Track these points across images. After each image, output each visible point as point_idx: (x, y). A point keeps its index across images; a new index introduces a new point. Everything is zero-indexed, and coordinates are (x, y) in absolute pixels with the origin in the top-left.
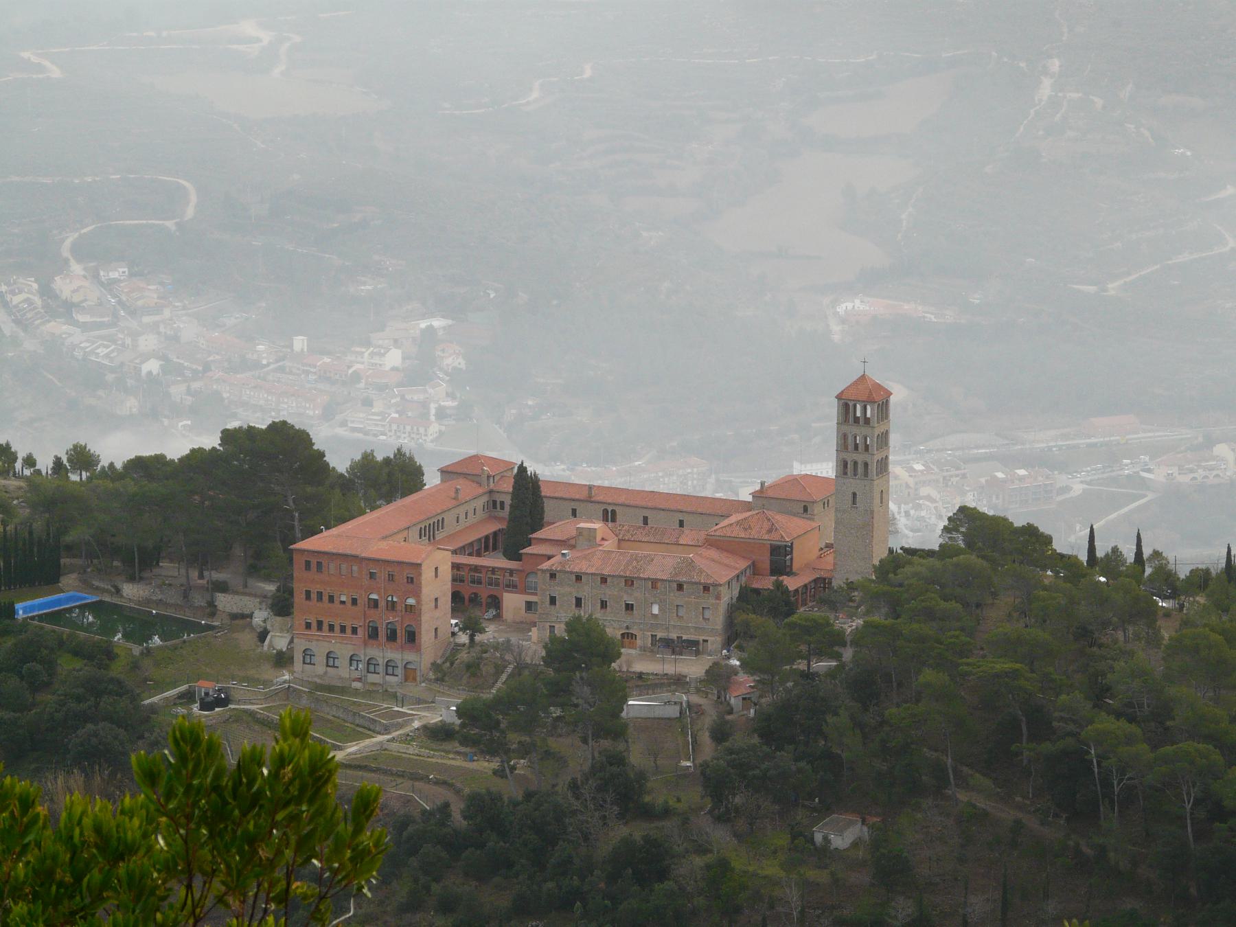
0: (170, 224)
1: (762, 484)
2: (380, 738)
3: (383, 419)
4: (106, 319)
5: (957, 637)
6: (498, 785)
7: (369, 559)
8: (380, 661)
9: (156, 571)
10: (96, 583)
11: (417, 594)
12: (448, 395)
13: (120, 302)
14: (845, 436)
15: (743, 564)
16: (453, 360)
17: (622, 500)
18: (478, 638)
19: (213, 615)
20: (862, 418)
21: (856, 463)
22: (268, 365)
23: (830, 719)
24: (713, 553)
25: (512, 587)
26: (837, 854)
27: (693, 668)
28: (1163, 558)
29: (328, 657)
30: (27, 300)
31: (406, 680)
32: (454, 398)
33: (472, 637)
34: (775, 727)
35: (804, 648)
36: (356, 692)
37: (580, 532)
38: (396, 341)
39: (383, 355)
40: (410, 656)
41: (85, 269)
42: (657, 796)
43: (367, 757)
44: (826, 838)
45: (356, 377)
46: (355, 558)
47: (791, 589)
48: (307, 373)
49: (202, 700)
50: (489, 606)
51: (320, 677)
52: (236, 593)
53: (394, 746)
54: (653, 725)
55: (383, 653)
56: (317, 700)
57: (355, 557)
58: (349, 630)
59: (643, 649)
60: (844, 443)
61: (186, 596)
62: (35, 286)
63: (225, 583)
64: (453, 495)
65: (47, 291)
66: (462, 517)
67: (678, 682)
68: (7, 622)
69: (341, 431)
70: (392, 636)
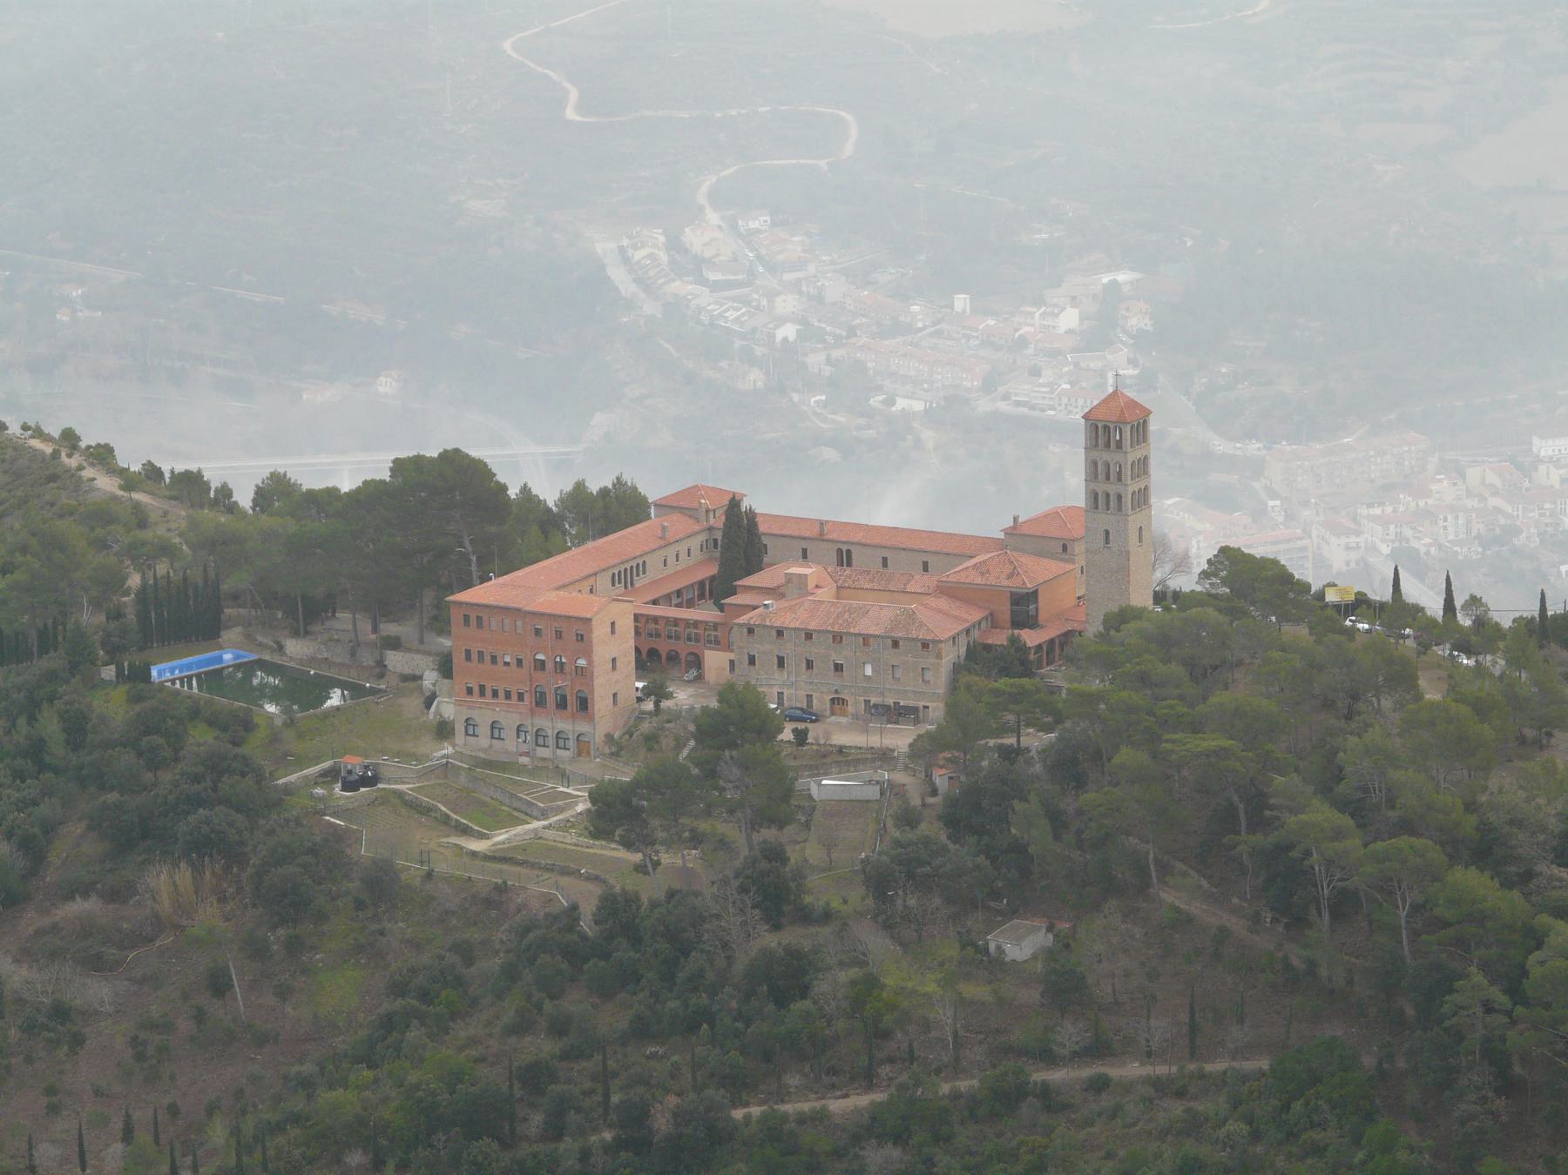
0: (823, 163)
1: (1015, 519)
2: (536, 824)
3: (1052, 392)
4: (741, 277)
5: (1172, 707)
6: (633, 883)
7: (533, 613)
8: (550, 733)
9: (328, 624)
10: (260, 638)
11: (588, 655)
12: (1130, 361)
13: (759, 257)
14: (1095, 463)
15: (976, 615)
16: (1138, 320)
17: (858, 537)
18: (665, 704)
19: (381, 676)
20: (1115, 434)
21: (1108, 495)
22: (924, 328)
23: (1018, 805)
24: (943, 603)
25: (716, 644)
26: (1013, 968)
27: (900, 739)
28: (1482, 605)
29: (492, 728)
30: (650, 256)
31: (579, 754)
32: (1136, 366)
33: (657, 704)
34: (972, 814)
35: (1011, 718)
36: (521, 769)
37: (790, 578)
38: (1074, 298)
39: (1057, 315)
40: (582, 727)
41: (722, 218)
42: (820, 893)
43: (515, 848)
44: (999, 948)
45: (1022, 342)
46: (517, 612)
47: (1029, 644)
48: (969, 337)
49: (344, 779)
50: (689, 665)
51: (485, 751)
52: (409, 650)
53: (549, 834)
54: (849, 808)
55: (552, 723)
56: (476, 779)
57: (519, 610)
58: (515, 697)
59: (856, 717)
60: (1095, 472)
61: (353, 655)
62: (662, 239)
63: (397, 638)
64: (660, 533)
65: (675, 245)
66: (671, 560)
67: (884, 757)
68: (142, 685)
69: (1002, 406)
70: (562, 704)
